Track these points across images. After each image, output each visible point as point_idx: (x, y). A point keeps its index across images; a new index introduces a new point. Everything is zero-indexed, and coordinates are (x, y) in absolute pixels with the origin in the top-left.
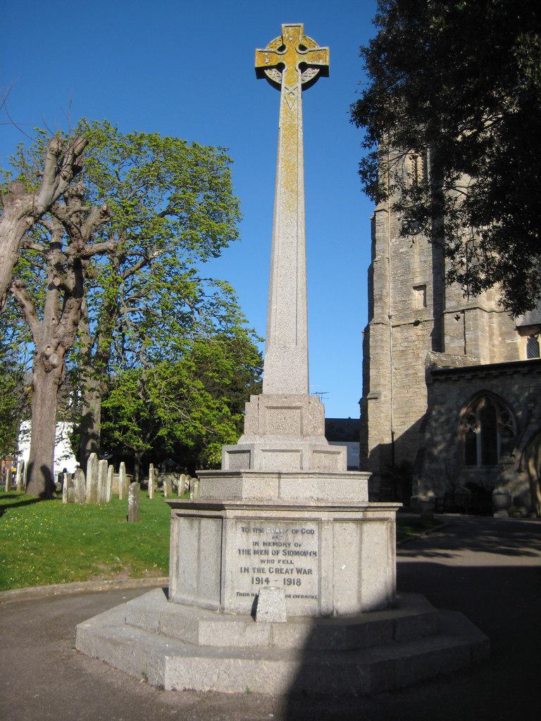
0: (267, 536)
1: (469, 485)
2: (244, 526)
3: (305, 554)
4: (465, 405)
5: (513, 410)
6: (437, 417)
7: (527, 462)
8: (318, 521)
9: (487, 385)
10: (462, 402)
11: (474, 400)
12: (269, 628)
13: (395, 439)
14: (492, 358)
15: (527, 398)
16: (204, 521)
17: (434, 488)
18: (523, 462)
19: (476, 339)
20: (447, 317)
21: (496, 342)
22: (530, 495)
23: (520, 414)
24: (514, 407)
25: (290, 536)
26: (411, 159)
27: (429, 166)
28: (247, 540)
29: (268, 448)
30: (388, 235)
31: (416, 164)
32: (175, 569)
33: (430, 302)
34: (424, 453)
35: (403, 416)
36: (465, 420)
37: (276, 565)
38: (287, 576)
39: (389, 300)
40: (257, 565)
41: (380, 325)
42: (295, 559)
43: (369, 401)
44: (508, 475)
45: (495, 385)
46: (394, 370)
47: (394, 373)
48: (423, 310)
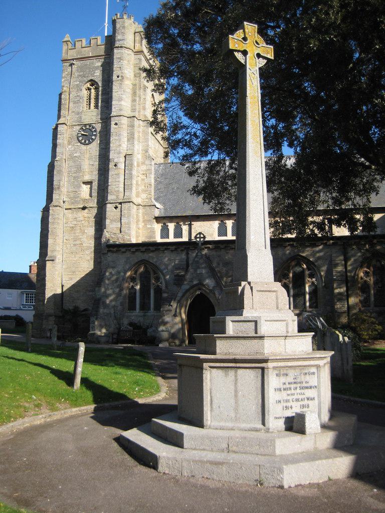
0: (290, 379)
1: (131, 324)
2: (277, 372)
3: (311, 387)
4: (129, 269)
5: (163, 274)
6: (109, 277)
7: (180, 310)
8: (318, 367)
9: (146, 256)
10: (127, 267)
11: (136, 266)
12: (314, 437)
13: (64, 290)
14: (137, 240)
15: (173, 266)
16: (240, 371)
17: (107, 326)
18: (178, 311)
19: (129, 223)
20: (108, 206)
21: (141, 226)
22: (181, 331)
23: (168, 277)
24: (164, 272)
25: (303, 376)
26: (86, 90)
27: (100, 97)
28: (280, 381)
29: (269, 319)
30: (66, 142)
31: (90, 94)
32: (209, 405)
33: (95, 194)
34: (98, 302)
35: (70, 274)
36: (129, 280)
37: (295, 397)
38: (302, 403)
39: (64, 190)
40: (286, 398)
41: (58, 208)
42: (306, 391)
43: (47, 262)
44: (167, 318)
45: (152, 257)
46: (65, 241)
47: (65, 243)
48: (89, 199)
